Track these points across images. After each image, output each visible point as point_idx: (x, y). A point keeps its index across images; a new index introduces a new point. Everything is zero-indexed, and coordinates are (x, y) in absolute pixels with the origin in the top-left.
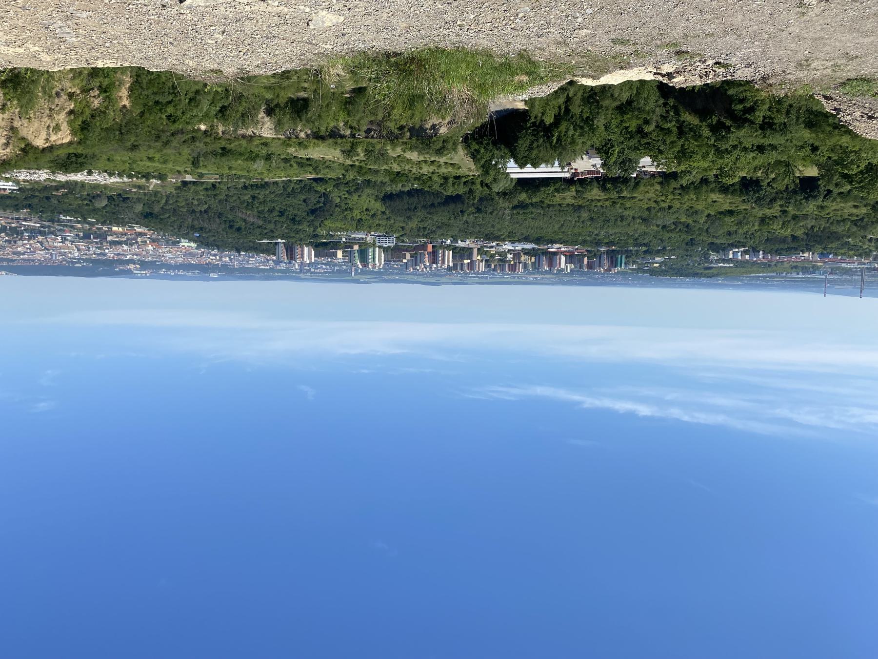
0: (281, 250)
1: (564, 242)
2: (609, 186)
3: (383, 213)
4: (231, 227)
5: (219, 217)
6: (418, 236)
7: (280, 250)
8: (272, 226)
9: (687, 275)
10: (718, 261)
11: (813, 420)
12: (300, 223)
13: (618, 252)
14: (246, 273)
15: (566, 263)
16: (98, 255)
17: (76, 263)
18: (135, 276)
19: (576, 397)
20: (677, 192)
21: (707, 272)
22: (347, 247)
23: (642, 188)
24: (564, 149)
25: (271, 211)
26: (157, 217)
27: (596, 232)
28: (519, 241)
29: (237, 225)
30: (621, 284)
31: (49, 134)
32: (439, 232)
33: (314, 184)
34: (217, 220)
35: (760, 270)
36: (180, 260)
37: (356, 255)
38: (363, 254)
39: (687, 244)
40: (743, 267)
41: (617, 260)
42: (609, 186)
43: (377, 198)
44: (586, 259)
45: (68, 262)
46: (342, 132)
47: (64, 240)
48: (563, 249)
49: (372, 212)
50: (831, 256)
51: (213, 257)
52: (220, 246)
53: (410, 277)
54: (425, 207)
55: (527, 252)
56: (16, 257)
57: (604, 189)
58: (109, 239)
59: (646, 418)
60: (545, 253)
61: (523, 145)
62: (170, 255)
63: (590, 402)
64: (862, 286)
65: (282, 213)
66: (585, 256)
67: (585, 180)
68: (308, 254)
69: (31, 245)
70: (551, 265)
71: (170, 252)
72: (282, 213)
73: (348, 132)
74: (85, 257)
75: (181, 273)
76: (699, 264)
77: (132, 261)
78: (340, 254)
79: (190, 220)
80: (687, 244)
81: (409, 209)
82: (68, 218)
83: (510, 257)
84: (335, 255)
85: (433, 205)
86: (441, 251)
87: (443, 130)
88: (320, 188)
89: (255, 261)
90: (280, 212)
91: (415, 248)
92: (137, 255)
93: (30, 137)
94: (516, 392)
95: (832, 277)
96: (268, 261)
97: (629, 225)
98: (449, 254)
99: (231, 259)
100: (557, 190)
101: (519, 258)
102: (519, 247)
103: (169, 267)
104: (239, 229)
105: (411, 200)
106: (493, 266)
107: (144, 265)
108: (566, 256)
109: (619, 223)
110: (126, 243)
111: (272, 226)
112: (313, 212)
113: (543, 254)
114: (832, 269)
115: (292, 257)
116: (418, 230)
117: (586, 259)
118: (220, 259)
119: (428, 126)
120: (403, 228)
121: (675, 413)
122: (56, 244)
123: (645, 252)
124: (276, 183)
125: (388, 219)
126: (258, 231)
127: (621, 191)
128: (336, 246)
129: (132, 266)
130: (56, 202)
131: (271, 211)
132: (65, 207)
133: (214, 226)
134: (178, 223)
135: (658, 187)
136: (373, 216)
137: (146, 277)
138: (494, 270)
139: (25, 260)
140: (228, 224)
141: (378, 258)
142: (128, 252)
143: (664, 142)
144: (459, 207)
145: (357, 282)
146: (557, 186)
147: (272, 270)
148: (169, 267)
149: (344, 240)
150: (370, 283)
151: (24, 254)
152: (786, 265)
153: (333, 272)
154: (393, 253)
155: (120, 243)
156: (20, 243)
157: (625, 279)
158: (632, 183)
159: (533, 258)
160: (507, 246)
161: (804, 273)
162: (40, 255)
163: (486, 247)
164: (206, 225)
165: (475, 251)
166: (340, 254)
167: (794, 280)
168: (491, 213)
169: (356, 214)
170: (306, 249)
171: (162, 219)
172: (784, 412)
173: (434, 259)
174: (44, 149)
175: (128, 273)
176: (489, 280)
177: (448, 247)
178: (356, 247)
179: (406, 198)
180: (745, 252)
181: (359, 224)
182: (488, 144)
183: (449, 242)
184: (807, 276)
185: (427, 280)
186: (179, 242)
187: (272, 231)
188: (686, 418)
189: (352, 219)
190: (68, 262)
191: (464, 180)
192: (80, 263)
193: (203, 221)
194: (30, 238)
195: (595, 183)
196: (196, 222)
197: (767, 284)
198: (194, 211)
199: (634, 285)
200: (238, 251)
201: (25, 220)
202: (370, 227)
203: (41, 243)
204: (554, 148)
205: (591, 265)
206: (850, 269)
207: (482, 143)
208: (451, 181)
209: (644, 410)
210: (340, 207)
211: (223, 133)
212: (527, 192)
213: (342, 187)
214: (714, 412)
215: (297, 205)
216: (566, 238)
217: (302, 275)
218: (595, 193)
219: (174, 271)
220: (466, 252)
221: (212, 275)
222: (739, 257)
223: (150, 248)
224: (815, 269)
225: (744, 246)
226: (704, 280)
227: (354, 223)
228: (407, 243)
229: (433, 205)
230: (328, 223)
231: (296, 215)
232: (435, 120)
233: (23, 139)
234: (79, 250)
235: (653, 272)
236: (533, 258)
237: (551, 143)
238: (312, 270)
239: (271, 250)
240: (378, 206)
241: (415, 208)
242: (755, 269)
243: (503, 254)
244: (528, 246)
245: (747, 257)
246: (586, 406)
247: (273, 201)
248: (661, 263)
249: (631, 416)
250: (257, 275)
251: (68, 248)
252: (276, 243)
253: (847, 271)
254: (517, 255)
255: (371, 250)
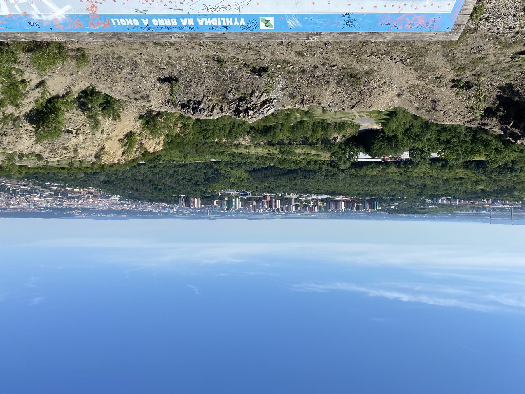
0: (182, 201)
1: (347, 195)
2: (402, 165)
3: (248, 179)
4: (155, 188)
5: (149, 183)
6: (264, 192)
7: (181, 201)
8: (180, 188)
9: (410, 213)
10: (429, 204)
11: (512, 302)
12: (199, 185)
13: (375, 200)
14: (144, 215)
15: (201, 204)
16: (57, 205)
17: (43, 210)
18: (76, 218)
19: (363, 289)
20: (439, 168)
21: (422, 211)
22: (220, 198)
23: (420, 166)
24: (398, 149)
25: (183, 179)
26: (112, 183)
27: (367, 189)
28: (321, 194)
29: (159, 187)
30: (365, 218)
31: (155, 146)
32: (278, 189)
33: (214, 164)
34: (148, 184)
35: (453, 209)
36: (106, 208)
37: (225, 203)
38: (229, 203)
39: (417, 195)
40: (443, 208)
41: (374, 204)
42: (402, 165)
43: (246, 171)
44: (356, 204)
45: (38, 210)
46: (284, 142)
47: (41, 196)
48: (344, 198)
49: (241, 179)
50: (499, 201)
51: (128, 205)
52: (133, 198)
53: (241, 215)
54: (274, 176)
55: (323, 200)
56: (7, 207)
57: (399, 167)
58: (69, 195)
59: (409, 303)
60: (333, 200)
61: (376, 147)
62: (101, 205)
63: (373, 293)
64: (512, 217)
65: (189, 180)
66: (355, 202)
67: (388, 162)
68: (197, 203)
69: (20, 200)
70: (336, 207)
71: (102, 203)
72: (189, 180)
73: (287, 142)
74: (49, 206)
75: (104, 215)
76: (418, 206)
77: (77, 209)
78: (215, 202)
79: (132, 185)
80: (417, 195)
81: (264, 177)
82: (53, 184)
83: (312, 203)
84: (213, 203)
85: (279, 175)
86: (274, 200)
87: (338, 140)
88: (216, 167)
89: (150, 207)
90: (188, 179)
91: (260, 199)
92: (81, 205)
93: (148, 148)
94: (321, 288)
95: (494, 213)
96: (159, 207)
97: (389, 185)
98: (278, 202)
99: (136, 207)
100: (372, 168)
101: (317, 204)
102: (320, 197)
103: (98, 211)
104: (160, 189)
105: (268, 172)
106: (299, 208)
107: (84, 210)
108: (344, 202)
109: (384, 184)
110: (78, 198)
111: (180, 188)
112: (208, 179)
113: (331, 201)
114: (494, 208)
115: (188, 204)
116: (265, 189)
117: (356, 204)
118: (131, 207)
119: (332, 138)
120: (257, 187)
121: (424, 299)
122: (35, 199)
123: (391, 200)
124: (191, 164)
125: (250, 182)
126: (172, 190)
127: (408, 168)
128: (214, 198)
129: (77, 211)
130: (52, 175)
131: (183, 179)
132: (57, 178)
133: (146, 188)
134: (124, 186)
135: (428, 166)
136: (242, 180)
137: (83, 218)
138: (299, 210)
139: (12, 209)
140: (154, 187)
141: (237, 204)
142: (76, 203)
143: (461, 146)
144: (295, 175)
145: (209, 218)
146: (372, 165)
147: (160, 212)
148: (98, 211)
149: (220, 194)
150: (217, 219)
151: (13, 205)
152: (468, 206)
153: (196, 212)
154: (246, 202)
155: (74, 198)
156: (14, 198)
157: (376, 216)
158: (415, 164)
159: (325, 204)
160: (314, 197)
161: (477, 211)
162: (23, 205)
163: (300, 197)
164: (141, 188)
165: (293, 200)
166: (215, 202)
167: (469, 215)
168: (312, 179)
169: (232, 180)
170: (196, 200)
171: (114, 184)
172: (492, 297)
173: (270, 204)
174: (152, 153)
175: (72, 216)
176: (288, 216)
177: (279, 198)
178: (226, 199)
179: (264, 171)
180: (449, 199)
181: (232, 186)
182: (352, 146)
183: (280, 195)
184: (478, 212)
185: (251, 217)
186: (110, 197)
187: (180, 190)
188: (431, 302)
189: (229, 183)
190: (38, 210)
191: (319, 162)
192: (45, 210)
193: (140, 185)
194: (21, 195)
195: (393, 164)
196: (135, 186)
197: (452, 218)
198: (135, 179)
199: (373, 219)
200: (152, 202)
201: (24, 185)
202: (238, 187)
203: (26, 199)
204: (392, 148)
205: (358, 208)
206: (505, 208)
207: (349, 145)
208: (312, 163)
209: (405, 298)
210: (224, 176)
211: (224, 143)
212: (355, 169)
213: (229, 166)
214: (447, 299)
215: (200, 176)
216: (349, 192)
217: (176, 215)
218: (393, 169)
219: (100, 214)
220: (288, 201)
221: (123, 216)
222: (445, 202)
223: (91, 200)
224: (484, 208)
225: (450, 196)
226: (415, 216)
227: (229, 185)
228: (256, 195)
229: (279, 175)
230: (215, 185)
231: (197, 181)
232: (335, 135)
233: (145, 149)
234: (48, 202)
235: (390, 211)
236: (325, 204)
237: (392, 145)
238: (184, 212)
239: (176, 201)
240: (246, 176)
241: (268, 176)
242: (450, 209)
243: (308, 202)
244: (325, 197)
245: (449, 202)
246: (371, 295)
247: (185, 174)
248: (395, 206)
249: (397, 301)
250: (150, 215)
251: (42, 201)
252: (179, 197)
253: (502, 210)
254: (316, 202)
255: (234, 200)
